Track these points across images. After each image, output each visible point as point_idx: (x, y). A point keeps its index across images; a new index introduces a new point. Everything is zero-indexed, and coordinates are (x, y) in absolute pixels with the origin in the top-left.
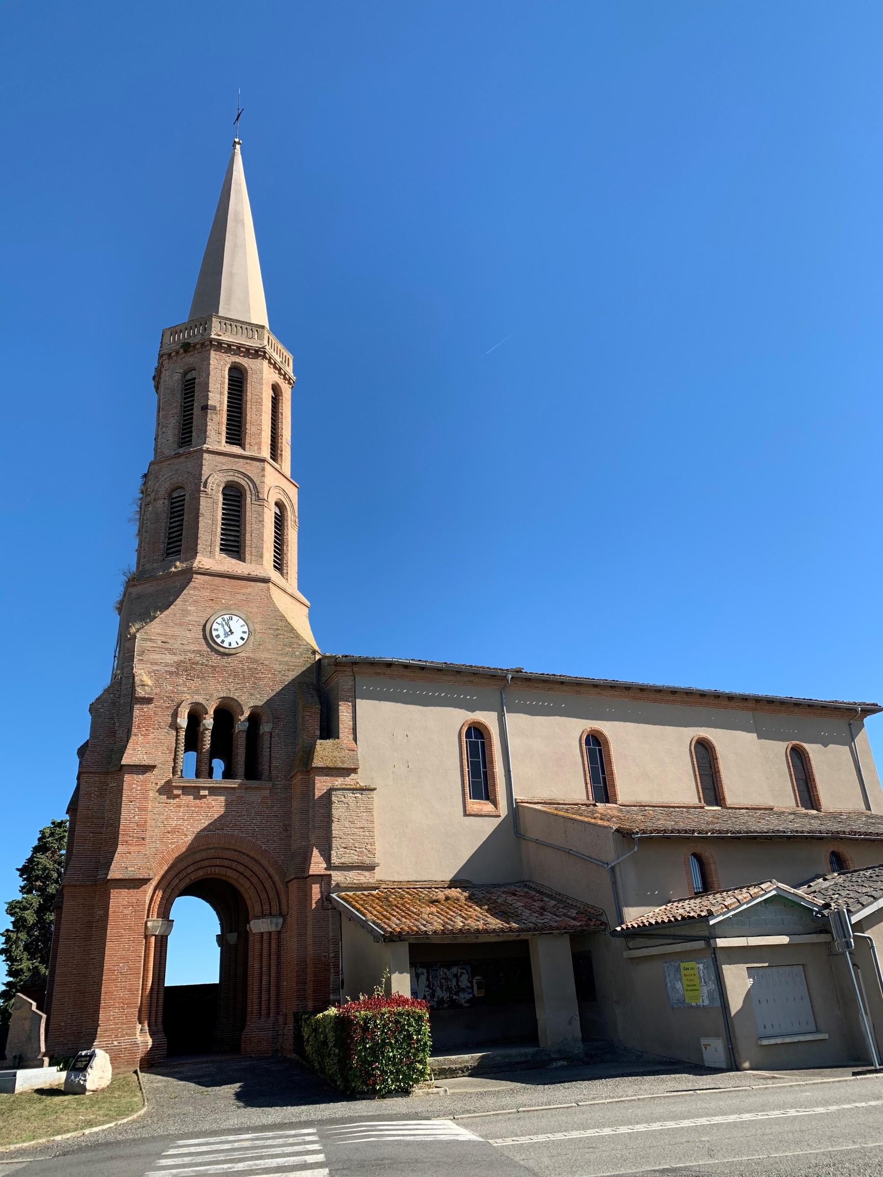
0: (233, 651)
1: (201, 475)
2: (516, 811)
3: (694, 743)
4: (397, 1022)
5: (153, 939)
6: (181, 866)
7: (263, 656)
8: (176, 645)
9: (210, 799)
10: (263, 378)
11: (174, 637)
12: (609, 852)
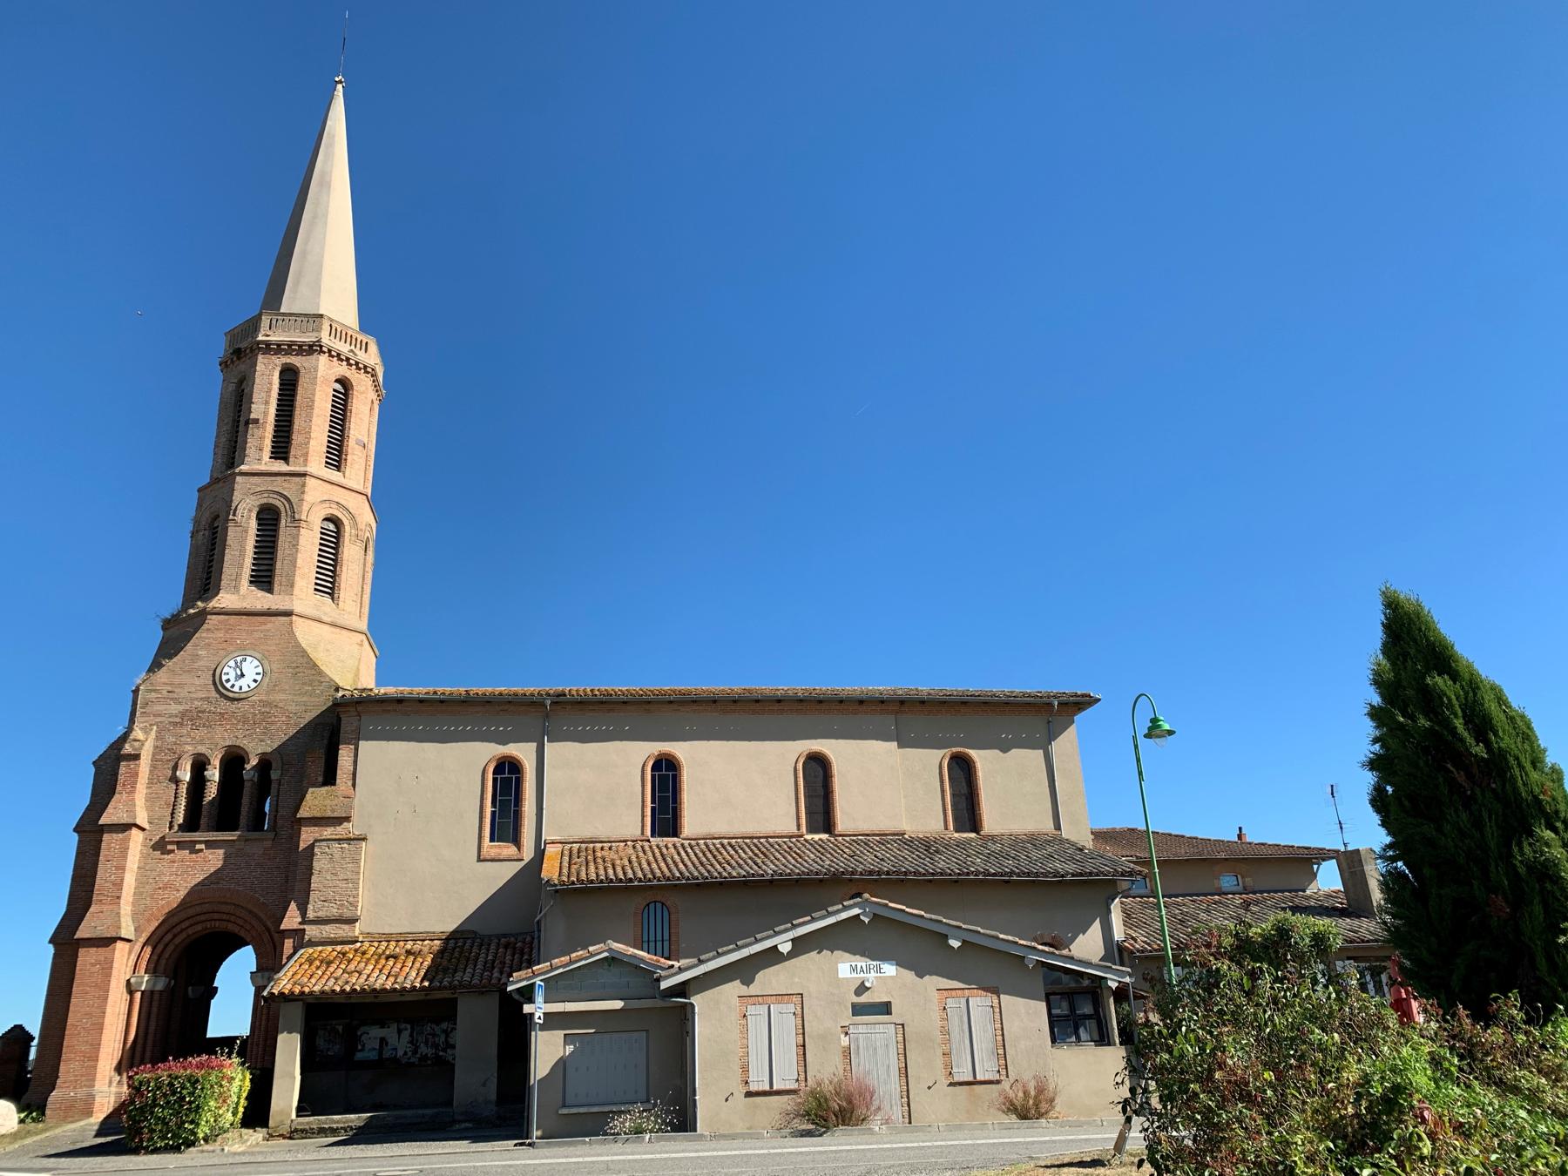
3: (801, 761)
4: (171, 1085)
5: (138, 995)
6: (175, 920)
7: (278, 697)
8: (183, 693)
9: (207, 852)
10: (321, 376)
11: (181, 685)
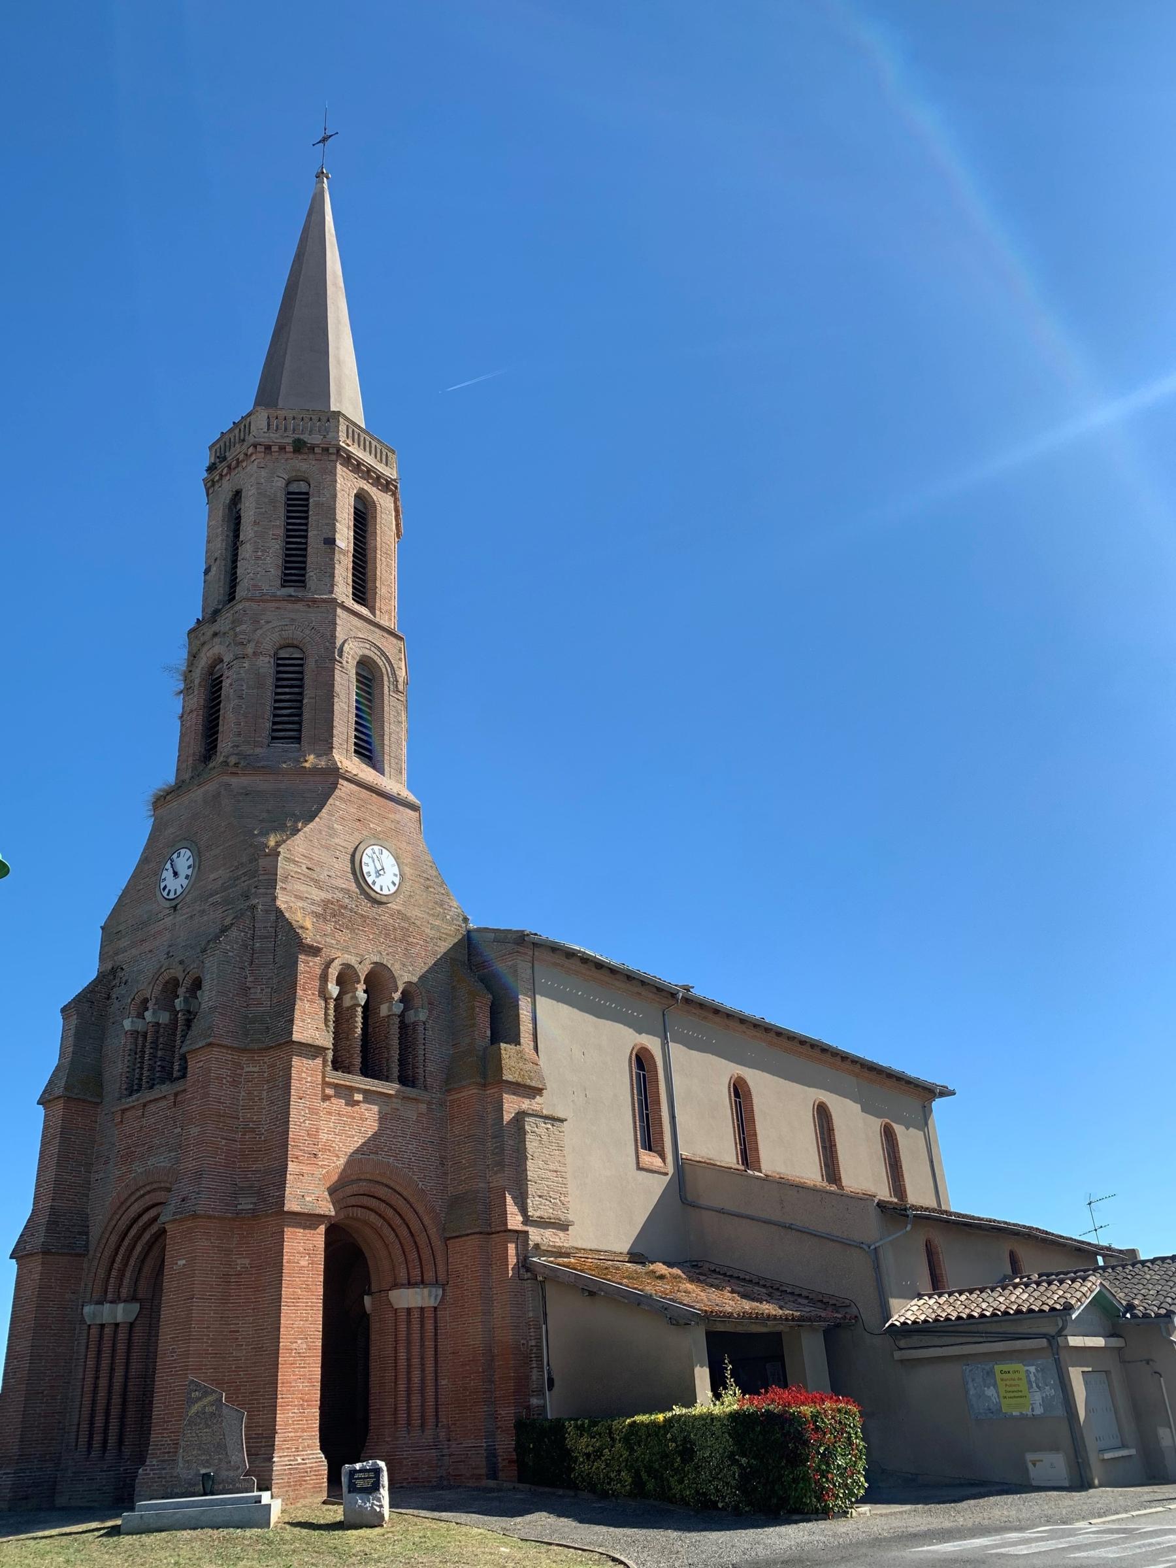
0: (384, 899)
1: (334, 637)
2: (682, 1167)
7: (414, 913)
9: (364, 1106)
11: (321, 864)
12: (870, 1229)
